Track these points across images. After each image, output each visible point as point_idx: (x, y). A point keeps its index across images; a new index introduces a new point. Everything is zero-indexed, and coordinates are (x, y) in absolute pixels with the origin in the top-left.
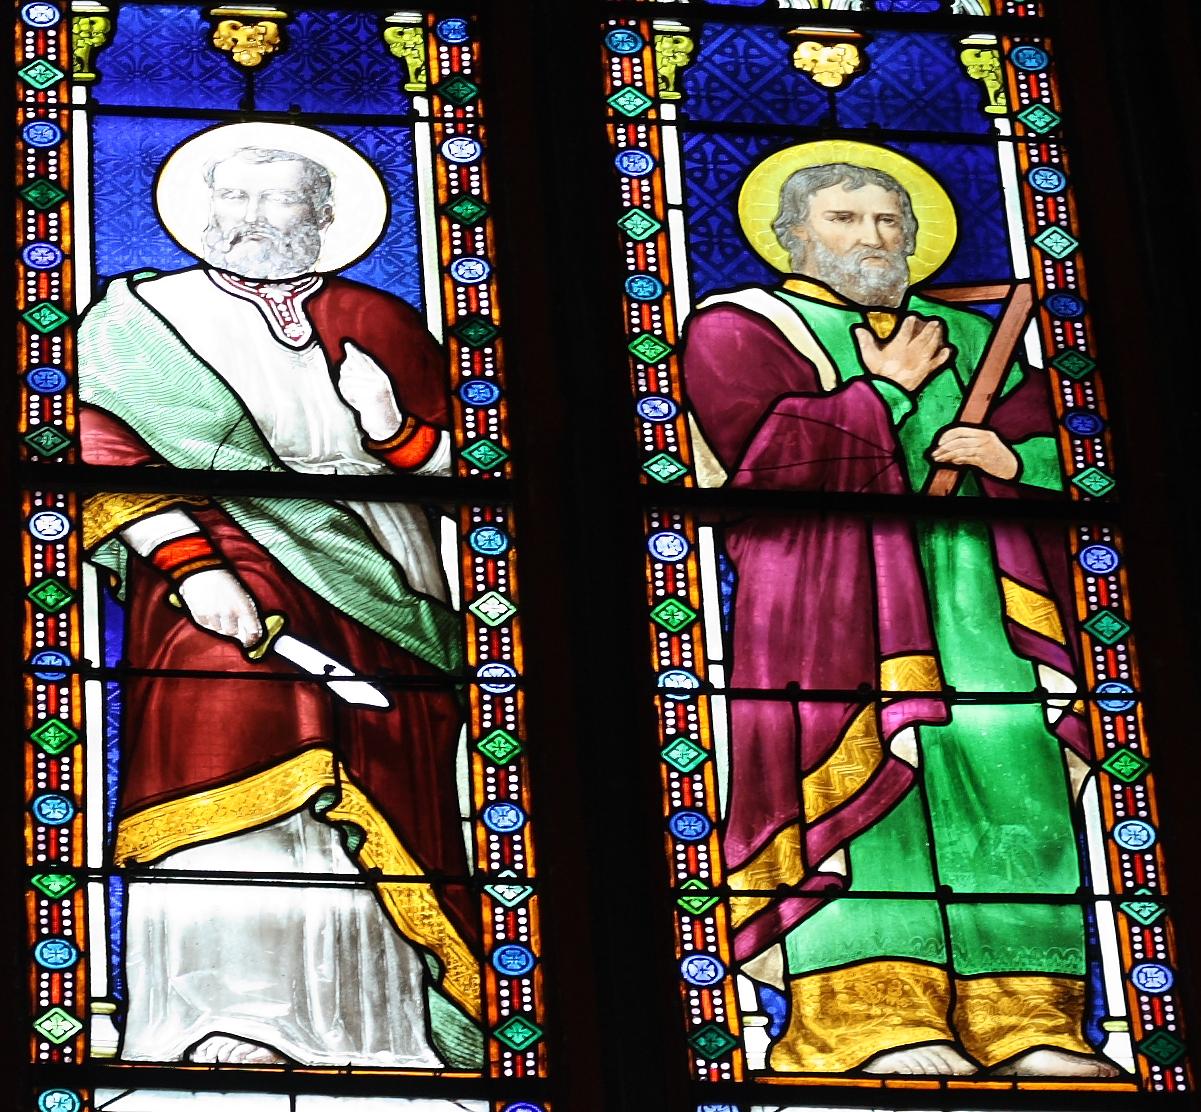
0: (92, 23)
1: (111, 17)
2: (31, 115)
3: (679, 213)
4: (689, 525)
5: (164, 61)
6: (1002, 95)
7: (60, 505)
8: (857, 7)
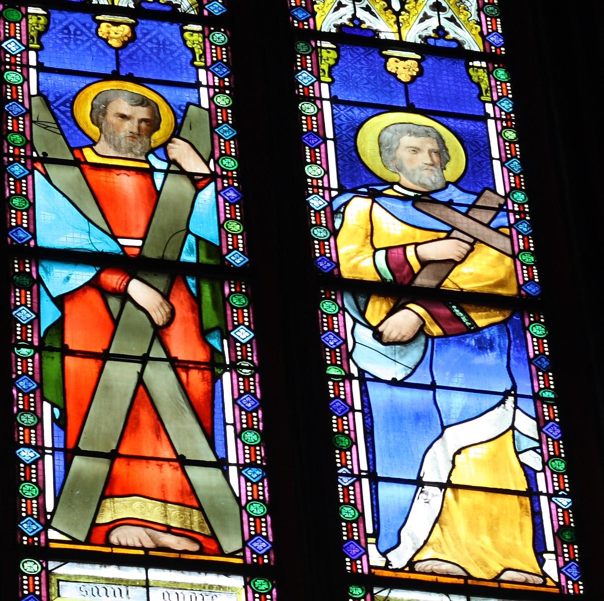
0: (39, 19)
1: (48, 16)
2: (504, 124)
3: (494, 156)
4: (339, 297)
5: (337, 72)
6: (203, 57)
7: (333, 297)
8: (132, 6)
